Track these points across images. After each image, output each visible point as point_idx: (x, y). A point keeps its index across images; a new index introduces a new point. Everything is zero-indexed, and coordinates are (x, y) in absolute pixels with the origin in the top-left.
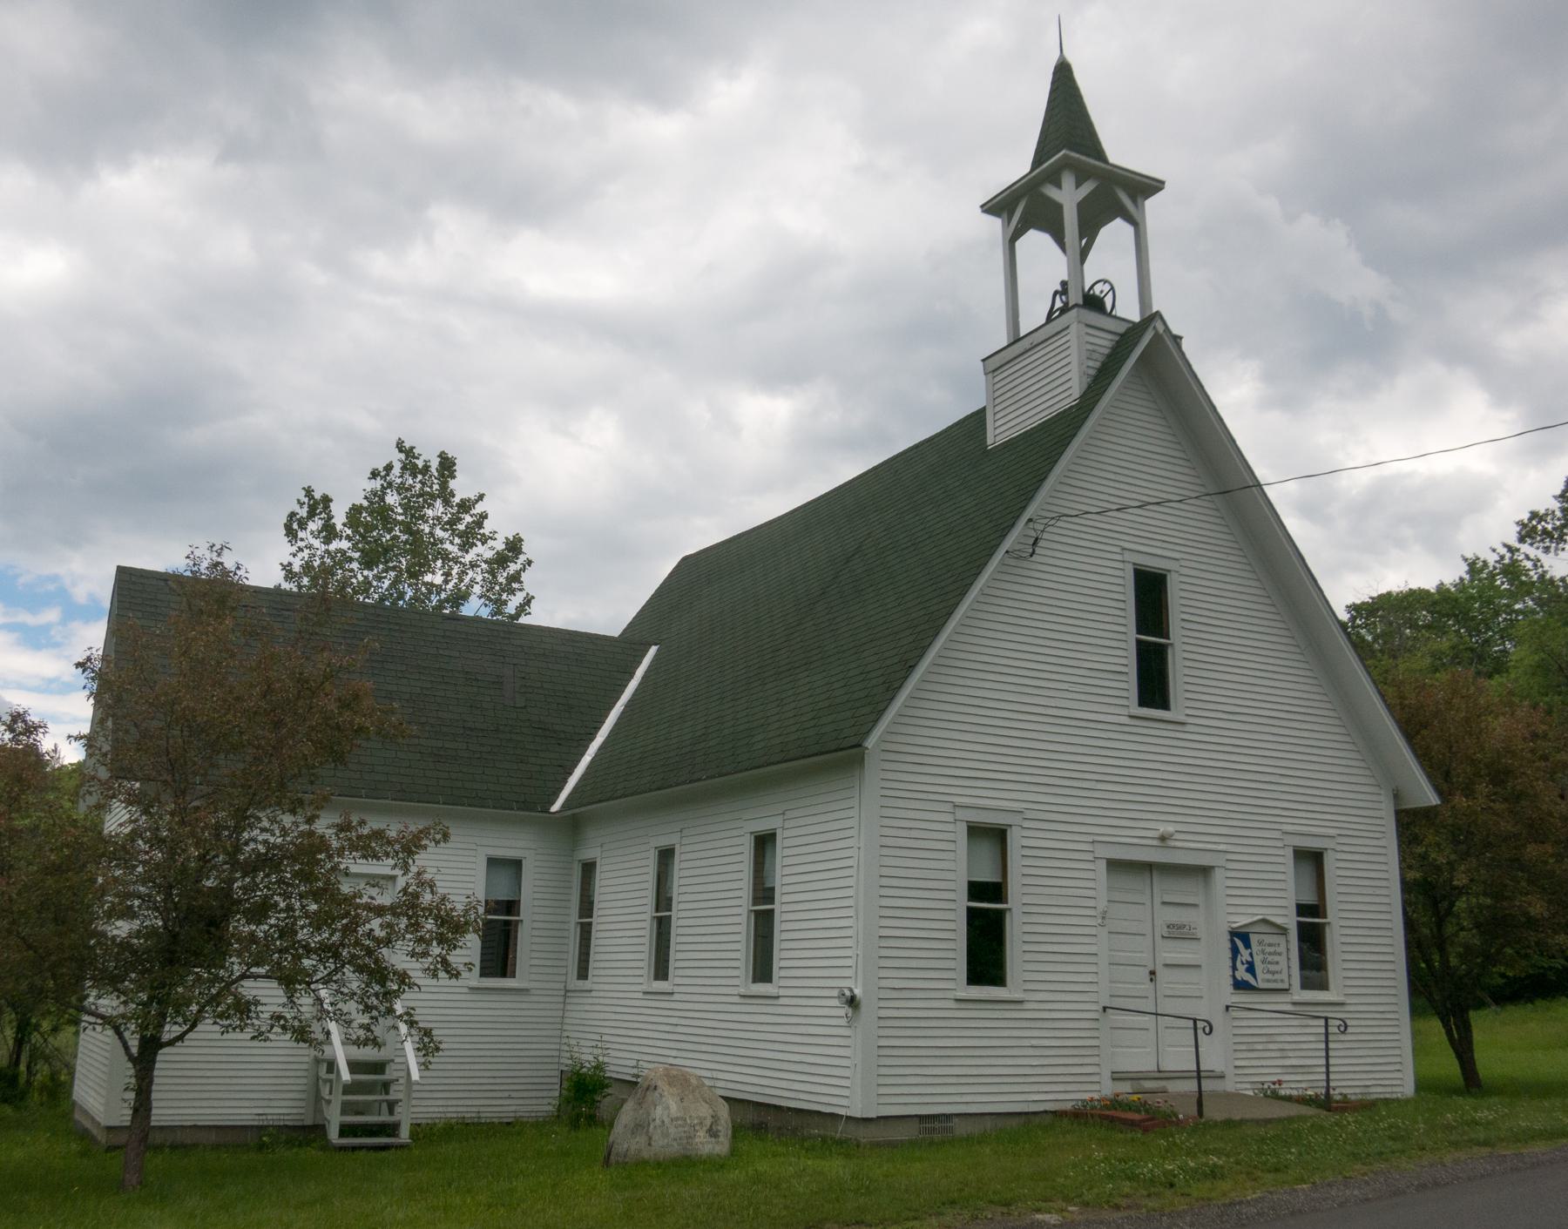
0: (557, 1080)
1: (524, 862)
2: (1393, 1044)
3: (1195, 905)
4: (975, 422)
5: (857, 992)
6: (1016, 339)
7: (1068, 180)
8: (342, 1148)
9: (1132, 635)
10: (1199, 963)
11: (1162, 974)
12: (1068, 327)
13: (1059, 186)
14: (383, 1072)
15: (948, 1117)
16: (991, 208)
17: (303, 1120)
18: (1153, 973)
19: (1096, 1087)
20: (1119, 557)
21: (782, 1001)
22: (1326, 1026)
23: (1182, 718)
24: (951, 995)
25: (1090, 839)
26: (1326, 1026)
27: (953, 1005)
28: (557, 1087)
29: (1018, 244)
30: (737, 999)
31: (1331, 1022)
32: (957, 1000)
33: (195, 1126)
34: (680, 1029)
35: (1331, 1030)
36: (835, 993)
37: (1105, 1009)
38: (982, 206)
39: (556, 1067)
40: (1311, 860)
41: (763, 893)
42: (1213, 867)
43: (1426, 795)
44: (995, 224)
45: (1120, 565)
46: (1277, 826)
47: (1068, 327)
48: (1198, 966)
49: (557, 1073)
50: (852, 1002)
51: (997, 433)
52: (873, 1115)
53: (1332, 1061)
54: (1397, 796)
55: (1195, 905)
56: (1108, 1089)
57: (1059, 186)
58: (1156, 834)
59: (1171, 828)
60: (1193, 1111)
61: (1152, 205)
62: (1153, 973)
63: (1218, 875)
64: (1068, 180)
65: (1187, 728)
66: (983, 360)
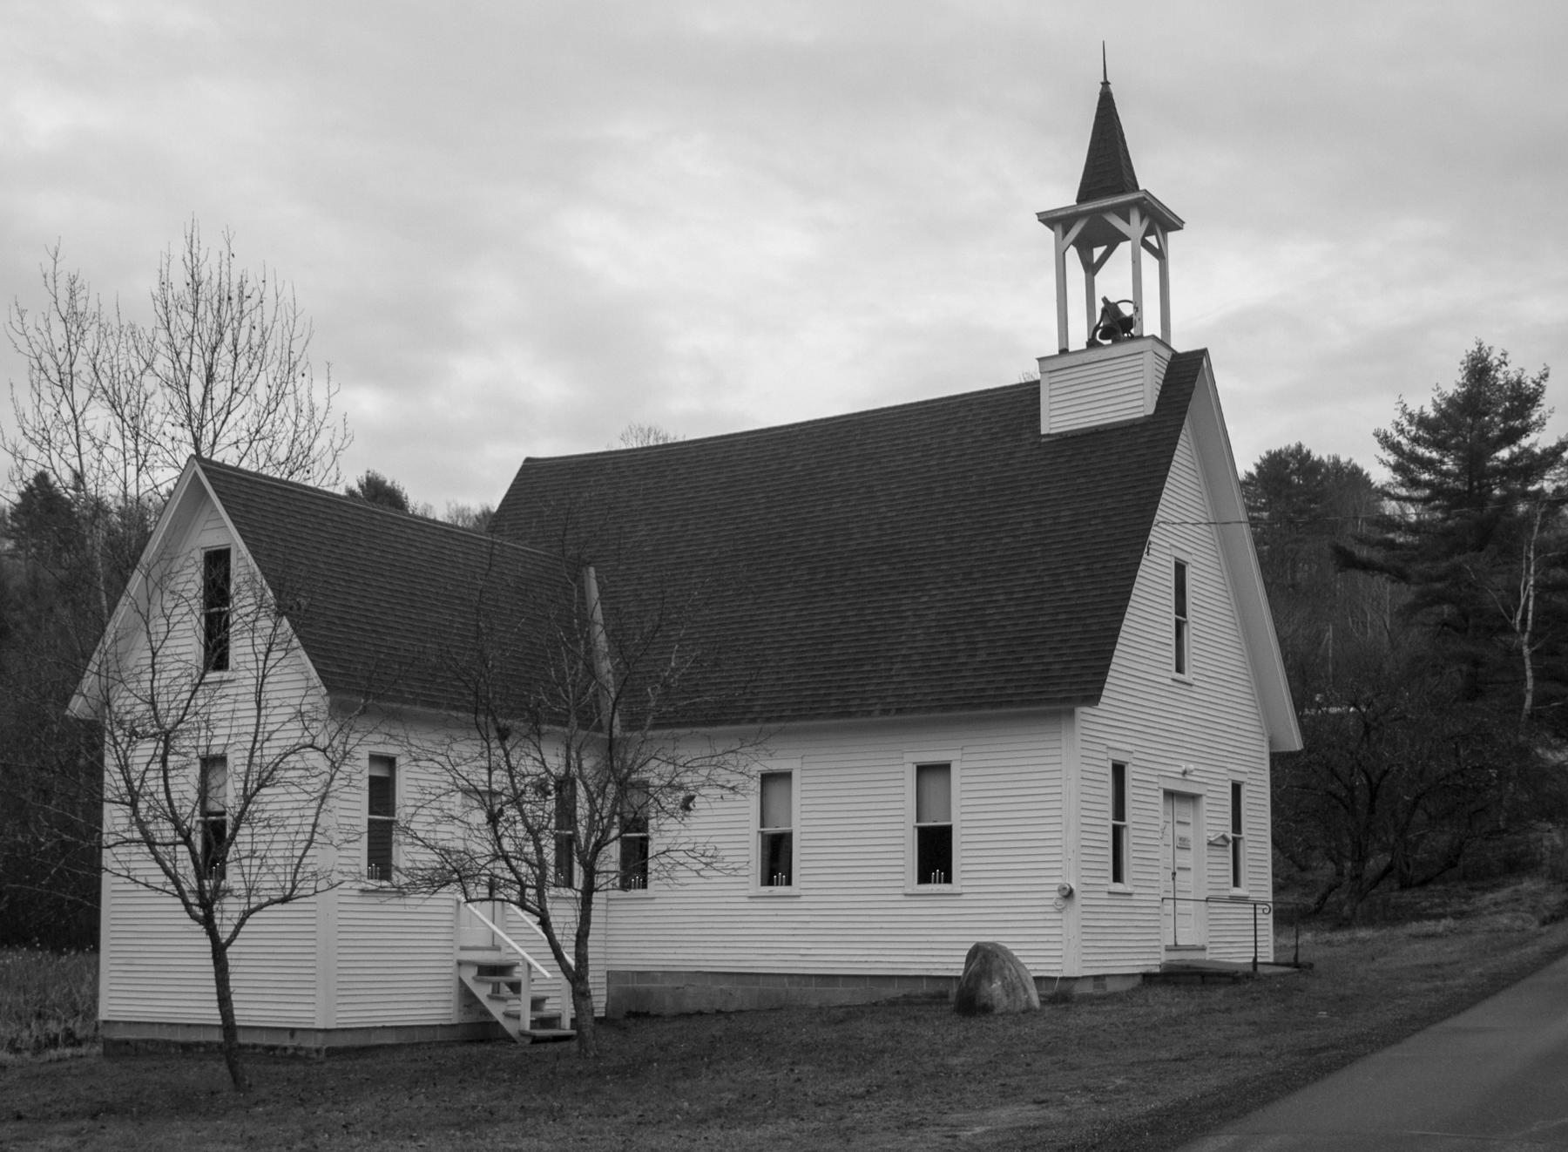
0: (604, 980)
1: (397, 760)
2: (310, 964)
3: (1188, 824)
4: (1024, 399)
5: (1073, 886)
6: (1064, 352)
7: (1135, 217)
8: (536, 1041)
9: (1173, 616)
10: (1189, 866)
11: (1179, 875)
12: (1142, 352)
13: (1128, 221)
14: (510, 975)
15: (1104, 976)
16: (1050, 220)
17: (450, 1019)
18: (1174, 874)
19: (1157, 956)
20: (1168, 552)
21: (964, 897)
22: (1255, 908)
23: (1191, 681)
24: (1106, 889)
25: (1157, 773)
26: (1255, 908)
27: (1106, 896)
28: (605, 986)
29: (1067, 253)
30: (746, 900)
31: (1258, 906)
32: (1110, 893)
33: (384, 1027)
34: (811, 925)
35: (1258, 911)
36: (1056, 888)
37: (1163, 899)
38: (1038, 214)
39: (602, 968)
40: (1236, 788)
41: (1119, 811)
42: (1200, 796)
43: (1295, 742)
44: (1048, 235)
45: (1168, 558)
46: (1224, 765)
47: (1142, 352)
48: (1189, 869)
49: (605, 974)
50: (1069, 895)
51: (1056, 419)
52: (1080, 975)
53: (1258, 939)
54: (1271, 743)
55: (1188, 824)
56: (1164, 957)
57: (1128, 221)
58: (1180, 770)
59: (1192, 766)
60: (1251, 969)
61: (1171, 235)
62: (1174, 874)
63: (1204, 800)
64: (1135, 217)
65: (1194, 688)
66: (1040, 360)
